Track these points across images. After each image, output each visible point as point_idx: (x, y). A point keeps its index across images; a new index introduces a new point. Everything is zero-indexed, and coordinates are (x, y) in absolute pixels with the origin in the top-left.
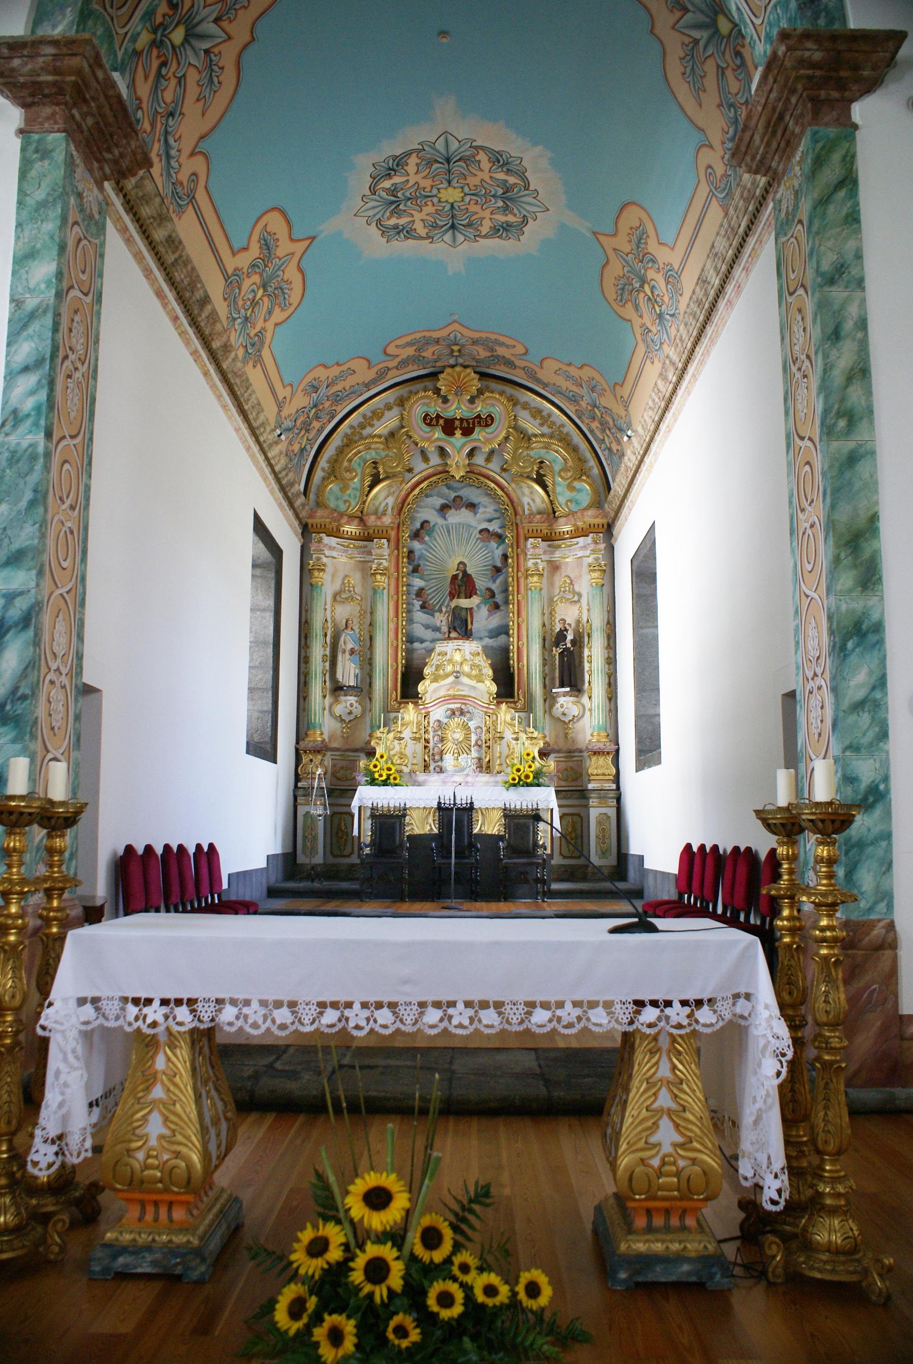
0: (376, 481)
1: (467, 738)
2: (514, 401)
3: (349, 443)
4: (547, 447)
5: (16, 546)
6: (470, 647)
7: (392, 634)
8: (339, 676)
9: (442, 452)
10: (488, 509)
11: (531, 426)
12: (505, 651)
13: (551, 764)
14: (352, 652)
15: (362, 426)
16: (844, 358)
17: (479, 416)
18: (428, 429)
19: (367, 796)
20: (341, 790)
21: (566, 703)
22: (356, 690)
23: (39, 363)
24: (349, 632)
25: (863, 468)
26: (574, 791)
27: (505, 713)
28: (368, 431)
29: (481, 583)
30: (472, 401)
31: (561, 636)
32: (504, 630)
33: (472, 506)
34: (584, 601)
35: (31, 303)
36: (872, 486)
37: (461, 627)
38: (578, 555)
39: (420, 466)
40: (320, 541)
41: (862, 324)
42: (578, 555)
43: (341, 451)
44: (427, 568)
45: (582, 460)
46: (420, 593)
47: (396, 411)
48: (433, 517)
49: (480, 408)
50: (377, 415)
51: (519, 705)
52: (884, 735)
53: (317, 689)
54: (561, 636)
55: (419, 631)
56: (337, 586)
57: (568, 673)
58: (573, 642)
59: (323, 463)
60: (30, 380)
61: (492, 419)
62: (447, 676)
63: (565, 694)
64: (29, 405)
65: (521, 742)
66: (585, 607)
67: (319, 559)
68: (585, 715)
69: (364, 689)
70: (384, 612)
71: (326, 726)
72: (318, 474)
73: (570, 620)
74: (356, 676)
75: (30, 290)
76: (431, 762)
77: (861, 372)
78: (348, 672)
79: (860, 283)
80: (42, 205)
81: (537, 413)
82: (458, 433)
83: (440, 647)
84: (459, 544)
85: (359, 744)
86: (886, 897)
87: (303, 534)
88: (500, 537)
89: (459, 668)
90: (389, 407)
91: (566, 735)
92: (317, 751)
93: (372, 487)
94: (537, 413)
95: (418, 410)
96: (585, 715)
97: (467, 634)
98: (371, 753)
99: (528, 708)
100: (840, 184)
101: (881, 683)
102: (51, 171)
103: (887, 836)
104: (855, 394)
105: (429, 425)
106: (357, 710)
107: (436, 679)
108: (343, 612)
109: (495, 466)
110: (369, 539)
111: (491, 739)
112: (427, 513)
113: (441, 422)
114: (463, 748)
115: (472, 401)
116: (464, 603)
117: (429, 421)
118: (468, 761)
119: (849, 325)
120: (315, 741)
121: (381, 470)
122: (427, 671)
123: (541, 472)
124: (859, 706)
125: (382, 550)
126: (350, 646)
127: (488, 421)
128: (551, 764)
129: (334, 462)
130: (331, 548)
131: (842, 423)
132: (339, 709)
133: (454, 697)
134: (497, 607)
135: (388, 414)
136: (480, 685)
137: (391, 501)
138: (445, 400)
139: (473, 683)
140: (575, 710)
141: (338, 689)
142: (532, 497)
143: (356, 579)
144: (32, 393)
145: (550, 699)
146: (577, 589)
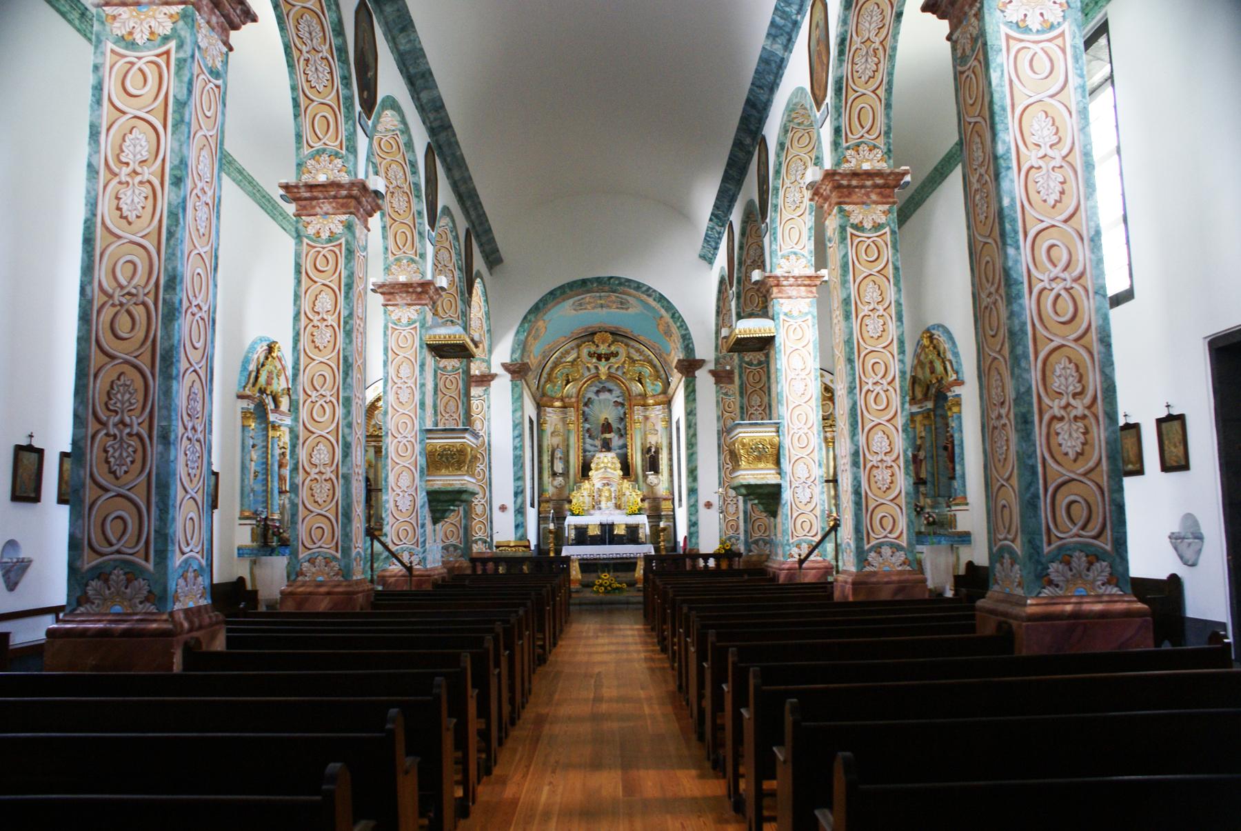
0: (568, 382)
3: (556, 365)
4: (643, 366)
10: (617, 392)
11: (636, 356)
12: (626, 455)
13: (646, 505)
16: (692, 432)
19: (570, 520)
20: (559, 518)
21: (652, 478)
26: (655, 516)
27: (626, 484)
29: (615, 426)
31: (649, 450)
32: (625, 446)
33: (610, 391)
36: (696, 460)
37: (607, 446)
38: (656, 413)
42: (656, 413)
43: (552, 369)
44: (591, 419)
45: (657, 371)
46: (588, 430)
48: (593, 396)
49: (613, 348)
54: (649, 450)
55: (588, 447)
59: (544, 375)
65: (633, 496)
68: (660, 483)
69: (565, 474)
70: (573, 440)
71: (550, 491)
72: (543, 380)
76: (596, 505)
77: (695, 435)
78: (559, 467)
81: (638, 350)
83: (598, 455)
84: (605, 410)
85: (564, 497)
88: (622, 405)
89: (606, 463)
92: (547, 501)
94: (638, 350)
95: (585, 351)
96: (660, 483)
97: (609, 449)
98: (570, 502)
99: (636, 481)
107: (597, 470)
108: (556, 441)
109: (619, 373)
110: (565, 407)
111: (620, 496)
112: (591, 395)
114: (609, 499)
116: (608, 436)
118: (611, 504)
122: (593, 466)
125: (572, 414)
127: (615, 355)
128: (646, 505)
129: (550, 374)
132: (556, 483)
134: (621, 436)
140: (656, 481)
142: (637, 388)
143: (560, 426)
145: (645, 477)
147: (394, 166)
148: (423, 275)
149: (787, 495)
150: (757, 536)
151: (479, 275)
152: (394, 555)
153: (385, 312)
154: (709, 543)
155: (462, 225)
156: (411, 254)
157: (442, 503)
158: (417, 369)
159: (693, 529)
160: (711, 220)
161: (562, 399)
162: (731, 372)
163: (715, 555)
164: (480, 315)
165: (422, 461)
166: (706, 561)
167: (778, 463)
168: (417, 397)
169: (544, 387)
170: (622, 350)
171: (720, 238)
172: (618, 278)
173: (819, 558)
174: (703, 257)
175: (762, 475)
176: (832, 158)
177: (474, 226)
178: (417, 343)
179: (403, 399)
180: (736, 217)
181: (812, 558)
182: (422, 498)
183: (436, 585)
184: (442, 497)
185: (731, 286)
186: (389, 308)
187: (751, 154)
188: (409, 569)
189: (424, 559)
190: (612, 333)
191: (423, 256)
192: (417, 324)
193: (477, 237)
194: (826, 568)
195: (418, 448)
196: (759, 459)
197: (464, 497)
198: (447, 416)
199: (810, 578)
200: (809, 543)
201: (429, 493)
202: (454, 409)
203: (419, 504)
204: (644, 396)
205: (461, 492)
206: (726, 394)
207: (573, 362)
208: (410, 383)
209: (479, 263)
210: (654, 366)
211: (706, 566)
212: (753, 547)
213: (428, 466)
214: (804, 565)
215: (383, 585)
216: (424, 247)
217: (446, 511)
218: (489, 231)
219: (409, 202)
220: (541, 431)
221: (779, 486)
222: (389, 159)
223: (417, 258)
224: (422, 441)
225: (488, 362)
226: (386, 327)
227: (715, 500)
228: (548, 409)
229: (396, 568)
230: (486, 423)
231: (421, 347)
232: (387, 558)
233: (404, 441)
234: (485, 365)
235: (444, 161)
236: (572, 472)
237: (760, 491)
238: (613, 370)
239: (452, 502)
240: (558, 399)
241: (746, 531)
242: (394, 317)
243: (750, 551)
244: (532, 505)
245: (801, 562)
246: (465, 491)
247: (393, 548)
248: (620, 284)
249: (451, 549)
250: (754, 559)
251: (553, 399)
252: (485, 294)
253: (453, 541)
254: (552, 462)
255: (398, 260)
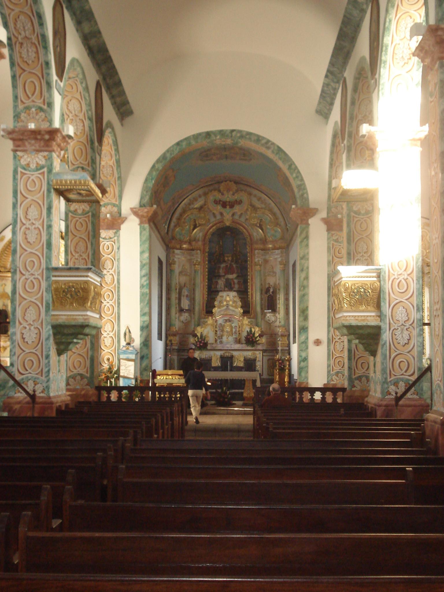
0: (195, 227)
1: (232, 330)
2: (250, 194)
3: (184, 211)
5: (144, 312)
6: (233, 294)
7: (202, 288)
8: (182, 306)
9: (221, 214)
11: (258, 204)
14: (187, 296)
15: (190, 204)
17: (236, 200)
18: (215, 205)
21: (269, 316)
22: (188, 311)
23: (147, 275)
24: (185, 288)
25: (306, 297)
28: (192, 206)
30: (233, 194)
31: (268, 290)
34: (277, 275)
35: (144, 262)
36: (308, 301)
39: (213, 220)
40: (174, 252)
41: (308, 268)
43: (181, 215)
47: (203, 198)
49: (236, 197)
50: (195, 199)
51: (252, 316)
52: (307, 348)
53: (173, 311)
54: (268, 290)
56: (180, 269)
57: (271, 305)
58: (273, 292)
59: (174, 220)
60: (145, 278)
61: (242, 202)
62: (223, 306)
63: (269, 313)
64: (145, 283)
66: (278, 278)
67: (173, 259)
69: (190, 311)
72: (172, 224)
73: (272, 283)
74: (189, 305)
75: (144, 260)
79: (308, 259)
80: (145, 241)
82: (228, 207)
86: (307, 378)
87: (167, 250)
90: (200, 196)
91: (270, 328)
92: (174, 335)
93: (193, 229)
94: (259, 199)
99: (255, 317)
100: (305, 238)
101: (307, 338)
102: (147, 233)
103: (307, 367)
104: (305, 282)
105: (216, 204)
106: (189, 318)
108: (183, 279)
110: (193, 250)
113: (221, 202)
114: (231, 333)
115: (233, 194)
117: (216, 202)
119: (305, 268)
120: (173, 331)
121: (197, 223)
123: (261, 223)
124: (303, 343)
126: (186, 293)
127: (240, 202)
129: (179, 219)
130: (178, 254)
131: (302, 288)
133: (226, 315)
135: (199, 200)
136: (236, 310)
137: (201, 234)
138: (223, 194)
139: (233, 309)
140: (273, 319)
141: (181, 310)
143: (187, 267)
144: (146, 281)
145: (264, 314)
146: (275, 270)
147: (22, 17)
148: (51, 121)
149: (386, 336)
150: (360, 372)
151: (110, 125)
152: (18, 384)
153: (15, 157)
154: (317, 376)
155: (93, 77)
156: (39, 103)
157: (66, 335)
158: (45, 212)
159: (302, 364)
160: (326, 76)
161: (190, 243)
162: (341, 221)
163: (323, 390)
164: (111, 163)
165: (48, 297)
166: (312, 395)
167: (378, 306)
168: (44, 238)
169: (173, 230)
170: (244, 197)
171: (335, 94)
172: (240, 131)
173: (415, 396)
174: (319, 112)
175: (365, 316)
176: (437, 14)
177: (104, 79)
178: (45, 187)
179: (31, 239)
180: (349, 74)
181: (409, 395)
182: (47, 331)
183: (59, 410)
184: (66, 331)
185: (343, 139)
186: (19, 153)
187: (363, 11)
188: (33, 397)
189: (48, 387)
190: (236, 183)
191: (50, 105)
192: (45, 170)
193: (108, 89)
194: (422, 406)
195: (44, 285)
196: (360, 302)
197: (87, 331)
198: (77, 256)
199: (406, 414)
200: (406, 381)
201: (54, 327)
202: (83, 249)
203: (44, 336)
204: (264, 241)
205: (83, 326)
206: (337, 241)
207: (201, 208)
208: (38, 224)
209: (109, 113)
210: (274, 214)
211: (312, 399)
212: (356, 383)
213: (53, 302)
214: (401, 403)
215: (9, 412)
216: (51, 96)
217: (70, 343)
218: (119, 83)
219: (37, 52)
220: (170, 271)
221: (379, 328)
222: (17, 10)
223: (45, 107)
224: (48, 278)
225: (119, 207)
226: (15, 172)
227: (324, 337)
228: (177, 251)
229: (21, 395)
230: (115, 263)
231: (49, 191)
232: (13, 386)
233: (32, 278)
234: (115, 209)
235: (73, 14)
236: (197, 308)
237: (361, 331)
238: (236, 217)
239: (75, 335)
240: (185, 243)
241: (350, 368)
242: (23, 162)
243: (354, 386)
244: (160, 338)
245: (398, 399)
246: (87, 326)
247: (18, 377)
248: (242, 137)
249: (78, 378)
250: (357, 394)
251: (181, 242)
252: (116, 143)
253: (82, 371)
254: (180, 300)
255: (28, 108)
